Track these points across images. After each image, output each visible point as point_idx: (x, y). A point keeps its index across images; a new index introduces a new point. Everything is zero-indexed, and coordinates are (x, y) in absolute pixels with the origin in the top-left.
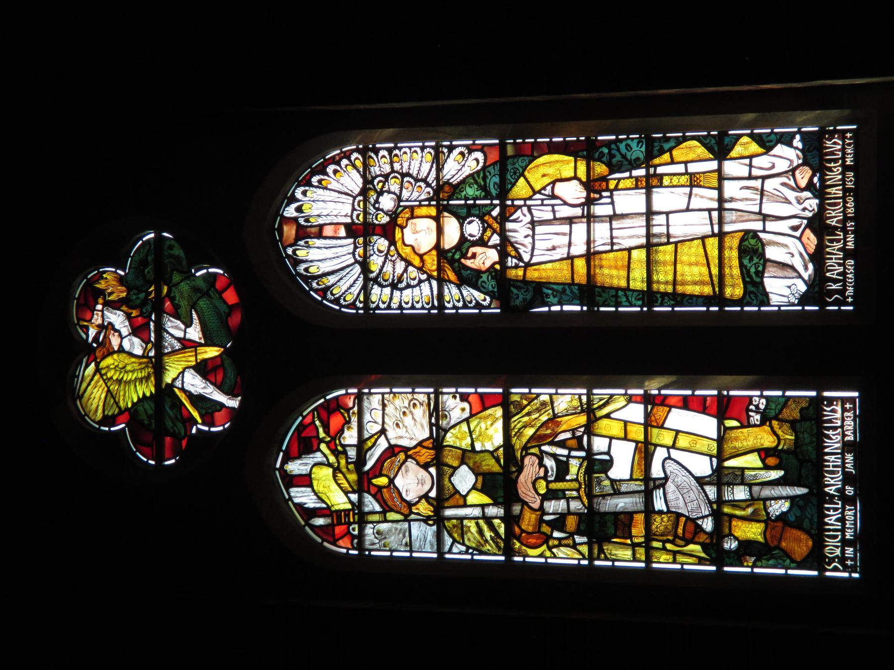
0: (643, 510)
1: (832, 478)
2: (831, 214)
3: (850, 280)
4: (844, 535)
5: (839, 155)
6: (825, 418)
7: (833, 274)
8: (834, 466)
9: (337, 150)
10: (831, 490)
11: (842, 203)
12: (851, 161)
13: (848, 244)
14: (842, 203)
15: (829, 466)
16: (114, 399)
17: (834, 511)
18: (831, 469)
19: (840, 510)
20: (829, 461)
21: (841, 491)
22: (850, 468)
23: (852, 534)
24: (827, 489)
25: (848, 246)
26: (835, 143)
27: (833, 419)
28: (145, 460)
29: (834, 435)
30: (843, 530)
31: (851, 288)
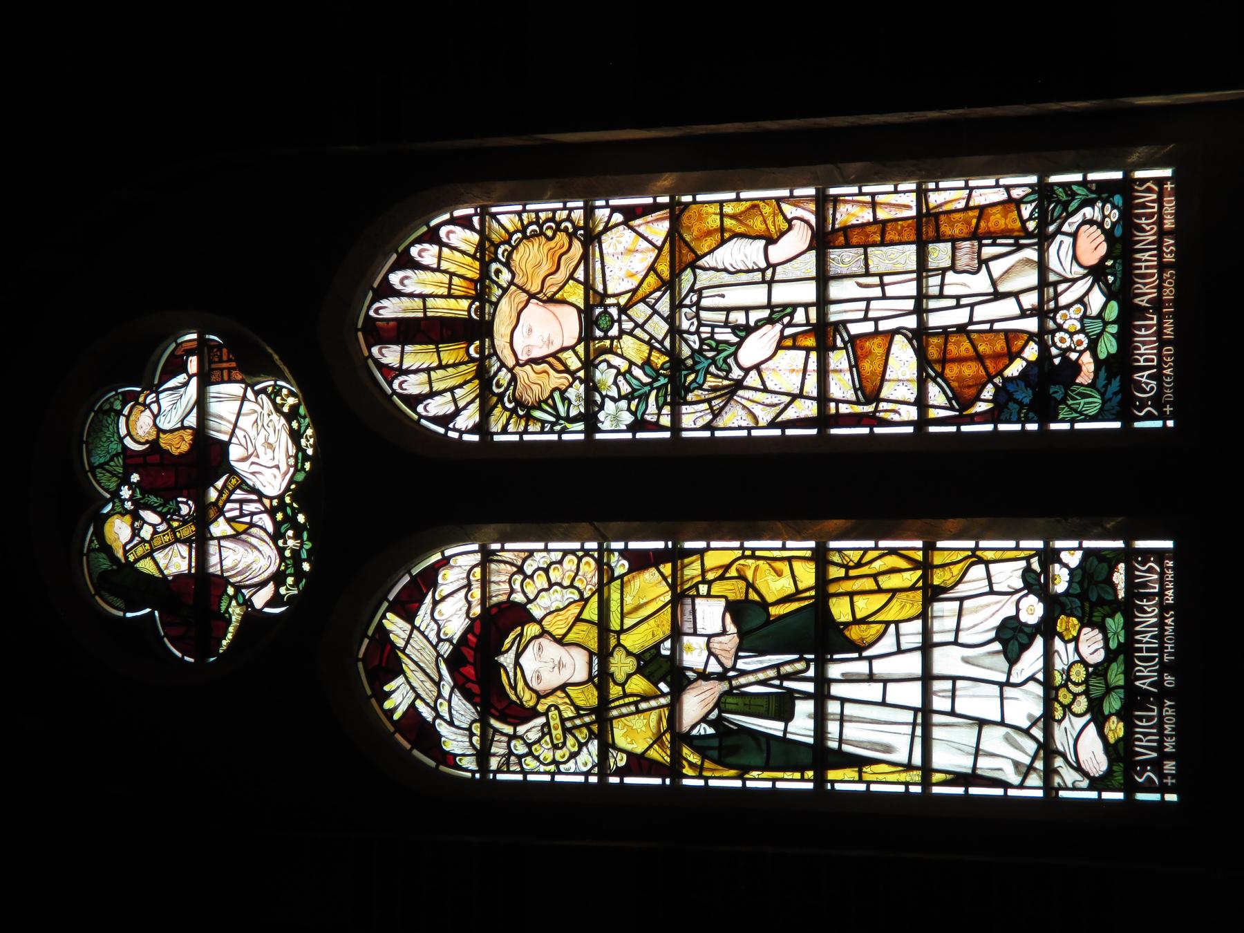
1: (1146, 667)
2: (1141, 289)
3: (1169, 380)
5: (1155, 588)
6: (1137, 201)
7: (1144, 684)
8: (1148, 650)
9: (445, 213)
10: (1142, 377)
11: (1156, 275)
12: (1172, 224)
14: (1156, 275)
15: (1140, 268)
17: (1145, 331)
18: (1143, 271)
21: (1159, 684)
22: (1169, 335)
24: (1137, 301)
26: (1150, 570)
27: (1148, 201)
28: (179, 655)
29: (1148, 225)
30: (1161, 650)
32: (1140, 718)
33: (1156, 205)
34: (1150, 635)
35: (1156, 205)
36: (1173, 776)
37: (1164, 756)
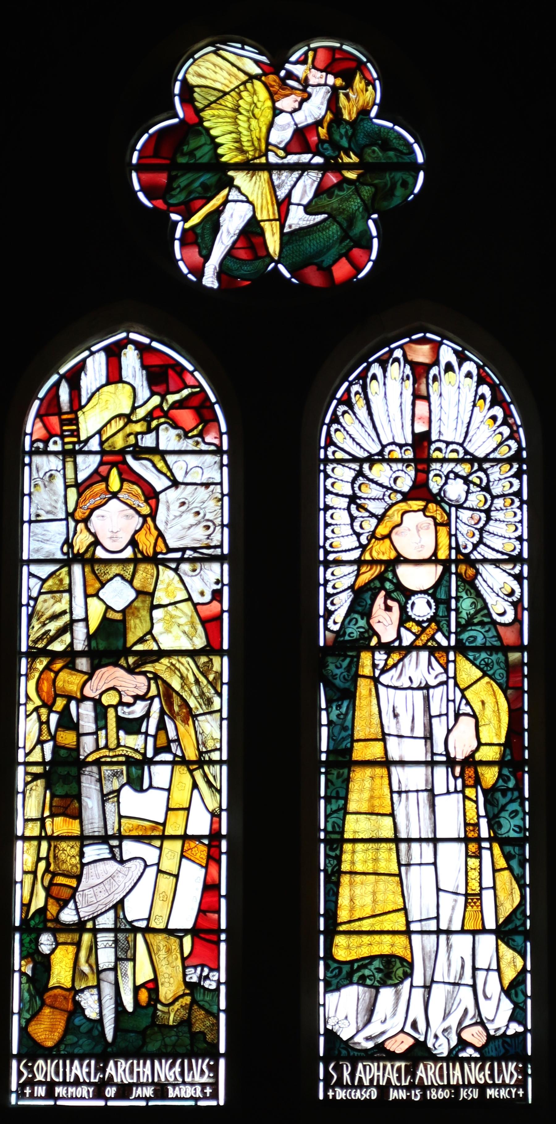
1: (434, 1073)
4: (59, 1084)
7: (360, 1073)
19: (87, 1081)
21: (110, 1082)
32: (89, 1065)
33: (500, 1082)
34: (424, 1076)
35: (500, 1082)
36: (334, 1096)
37: (424, 1088)
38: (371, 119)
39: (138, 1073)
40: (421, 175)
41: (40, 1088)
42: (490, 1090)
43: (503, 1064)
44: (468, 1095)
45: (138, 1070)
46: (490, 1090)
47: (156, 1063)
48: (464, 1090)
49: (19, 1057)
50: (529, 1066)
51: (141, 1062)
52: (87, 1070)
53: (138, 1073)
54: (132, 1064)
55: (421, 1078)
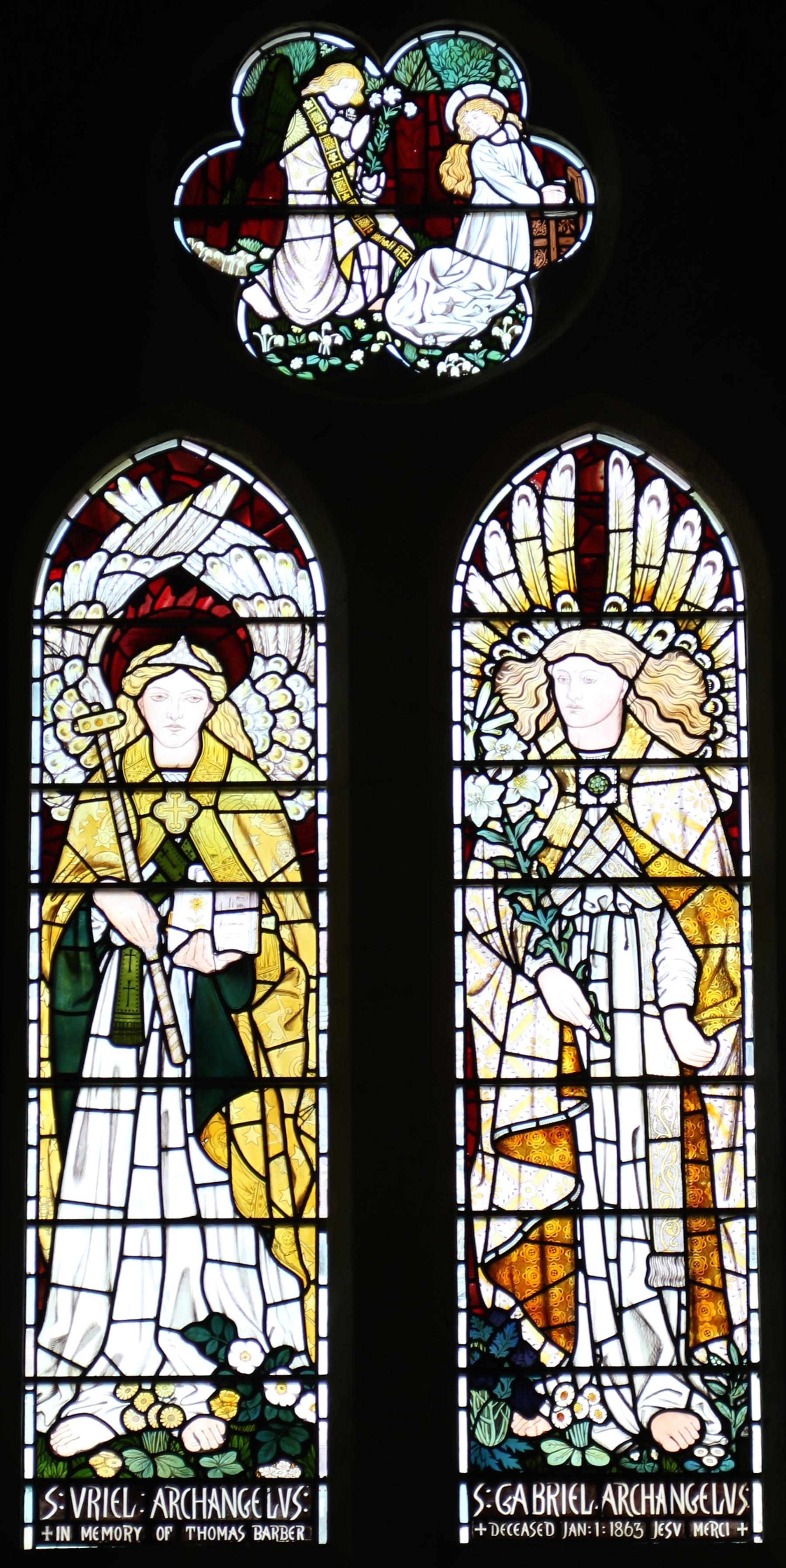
0: (54, 1133)
1: (628, 1499)
4: (191, 1522)
8: (199, 1506)
13: (573, 1525)
15: (648, 1492)
16: (341, 273)
17: (116, 1505)
19: (576, 1512)
20: (656, 1492)
21: (160, 1519)
23: (205, 1538)
25: (569, 1527)
26: (293, 1508)
30: (200, 1522)
31: (502, 1529)
33: (721, 1512)
34: (163, 1507)
38: (243, 140)
39: (648, 1501)
40: (590, 217)
41: (63, 1528)
42: (698, 1525)
43: (725, 1486)
44: (665, 1532)
45: (648, 1497)
46: (698, 1525)
47: (224, 1492)
48: (659, 1524)
49: (471, 1479)
50: (269, 1490)
51: (652, 1486)
52: (575, 1498)
53: (648, 1501)
54: (189, 1494)
55: (159, 1509)
